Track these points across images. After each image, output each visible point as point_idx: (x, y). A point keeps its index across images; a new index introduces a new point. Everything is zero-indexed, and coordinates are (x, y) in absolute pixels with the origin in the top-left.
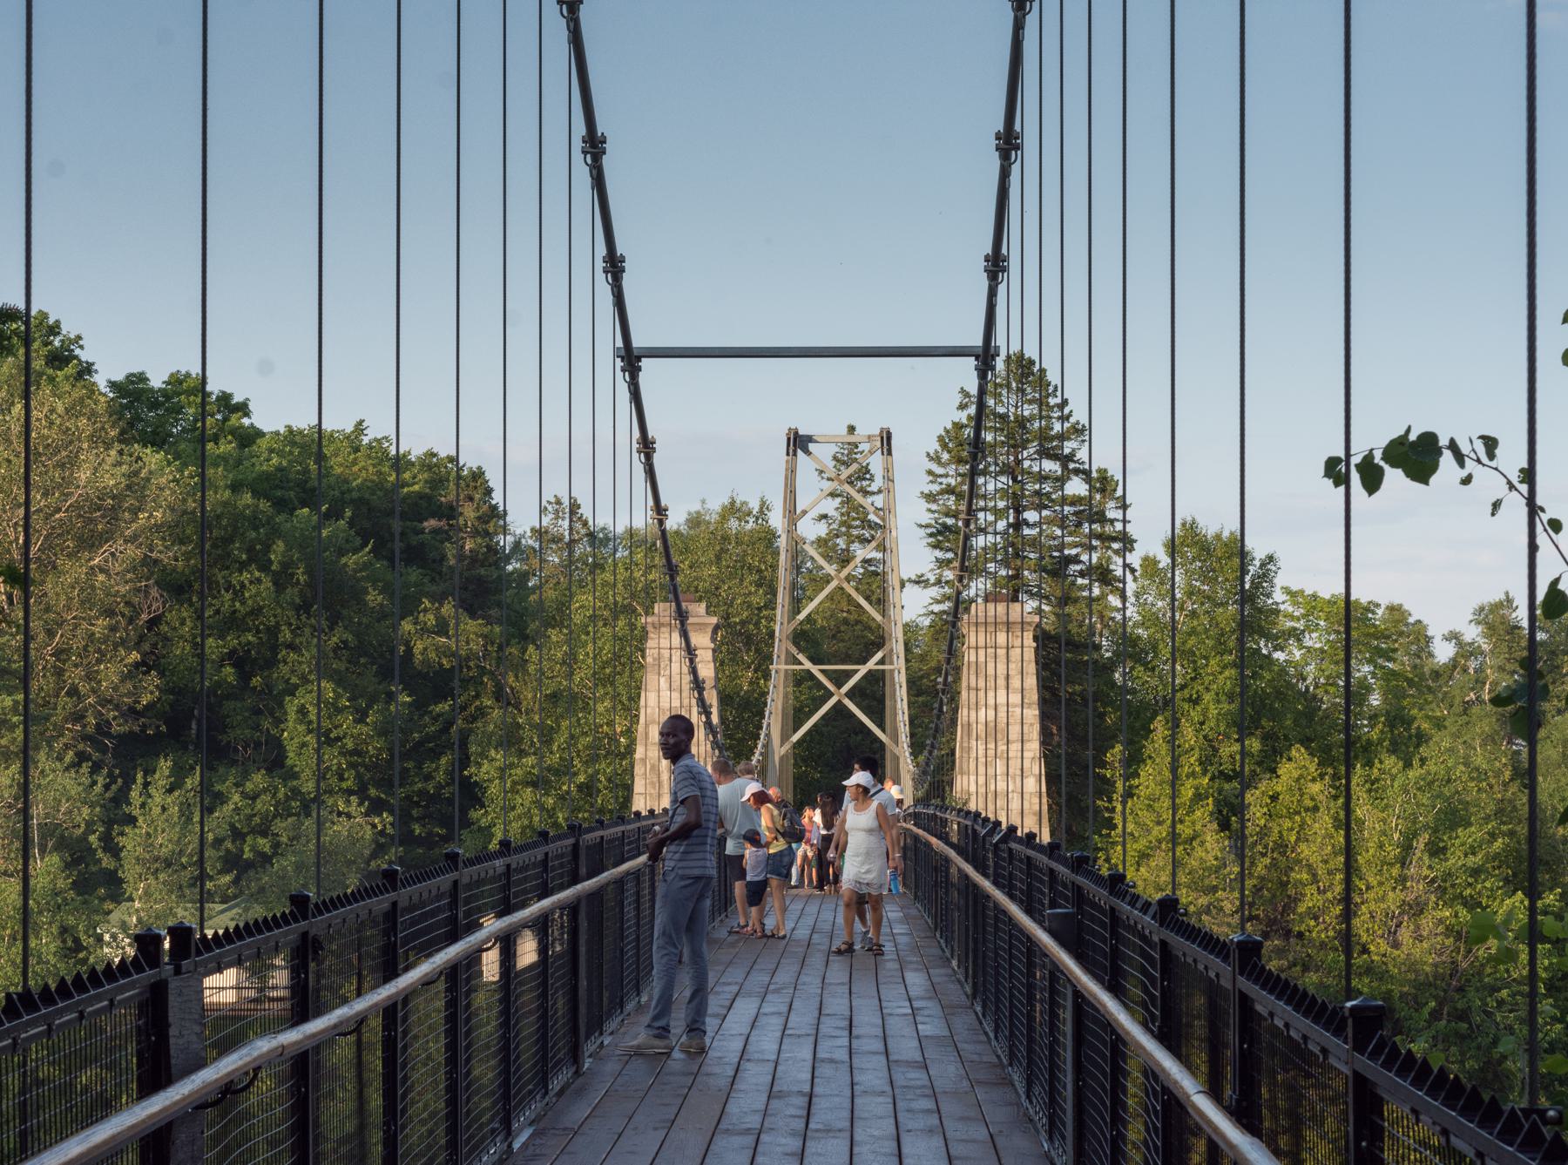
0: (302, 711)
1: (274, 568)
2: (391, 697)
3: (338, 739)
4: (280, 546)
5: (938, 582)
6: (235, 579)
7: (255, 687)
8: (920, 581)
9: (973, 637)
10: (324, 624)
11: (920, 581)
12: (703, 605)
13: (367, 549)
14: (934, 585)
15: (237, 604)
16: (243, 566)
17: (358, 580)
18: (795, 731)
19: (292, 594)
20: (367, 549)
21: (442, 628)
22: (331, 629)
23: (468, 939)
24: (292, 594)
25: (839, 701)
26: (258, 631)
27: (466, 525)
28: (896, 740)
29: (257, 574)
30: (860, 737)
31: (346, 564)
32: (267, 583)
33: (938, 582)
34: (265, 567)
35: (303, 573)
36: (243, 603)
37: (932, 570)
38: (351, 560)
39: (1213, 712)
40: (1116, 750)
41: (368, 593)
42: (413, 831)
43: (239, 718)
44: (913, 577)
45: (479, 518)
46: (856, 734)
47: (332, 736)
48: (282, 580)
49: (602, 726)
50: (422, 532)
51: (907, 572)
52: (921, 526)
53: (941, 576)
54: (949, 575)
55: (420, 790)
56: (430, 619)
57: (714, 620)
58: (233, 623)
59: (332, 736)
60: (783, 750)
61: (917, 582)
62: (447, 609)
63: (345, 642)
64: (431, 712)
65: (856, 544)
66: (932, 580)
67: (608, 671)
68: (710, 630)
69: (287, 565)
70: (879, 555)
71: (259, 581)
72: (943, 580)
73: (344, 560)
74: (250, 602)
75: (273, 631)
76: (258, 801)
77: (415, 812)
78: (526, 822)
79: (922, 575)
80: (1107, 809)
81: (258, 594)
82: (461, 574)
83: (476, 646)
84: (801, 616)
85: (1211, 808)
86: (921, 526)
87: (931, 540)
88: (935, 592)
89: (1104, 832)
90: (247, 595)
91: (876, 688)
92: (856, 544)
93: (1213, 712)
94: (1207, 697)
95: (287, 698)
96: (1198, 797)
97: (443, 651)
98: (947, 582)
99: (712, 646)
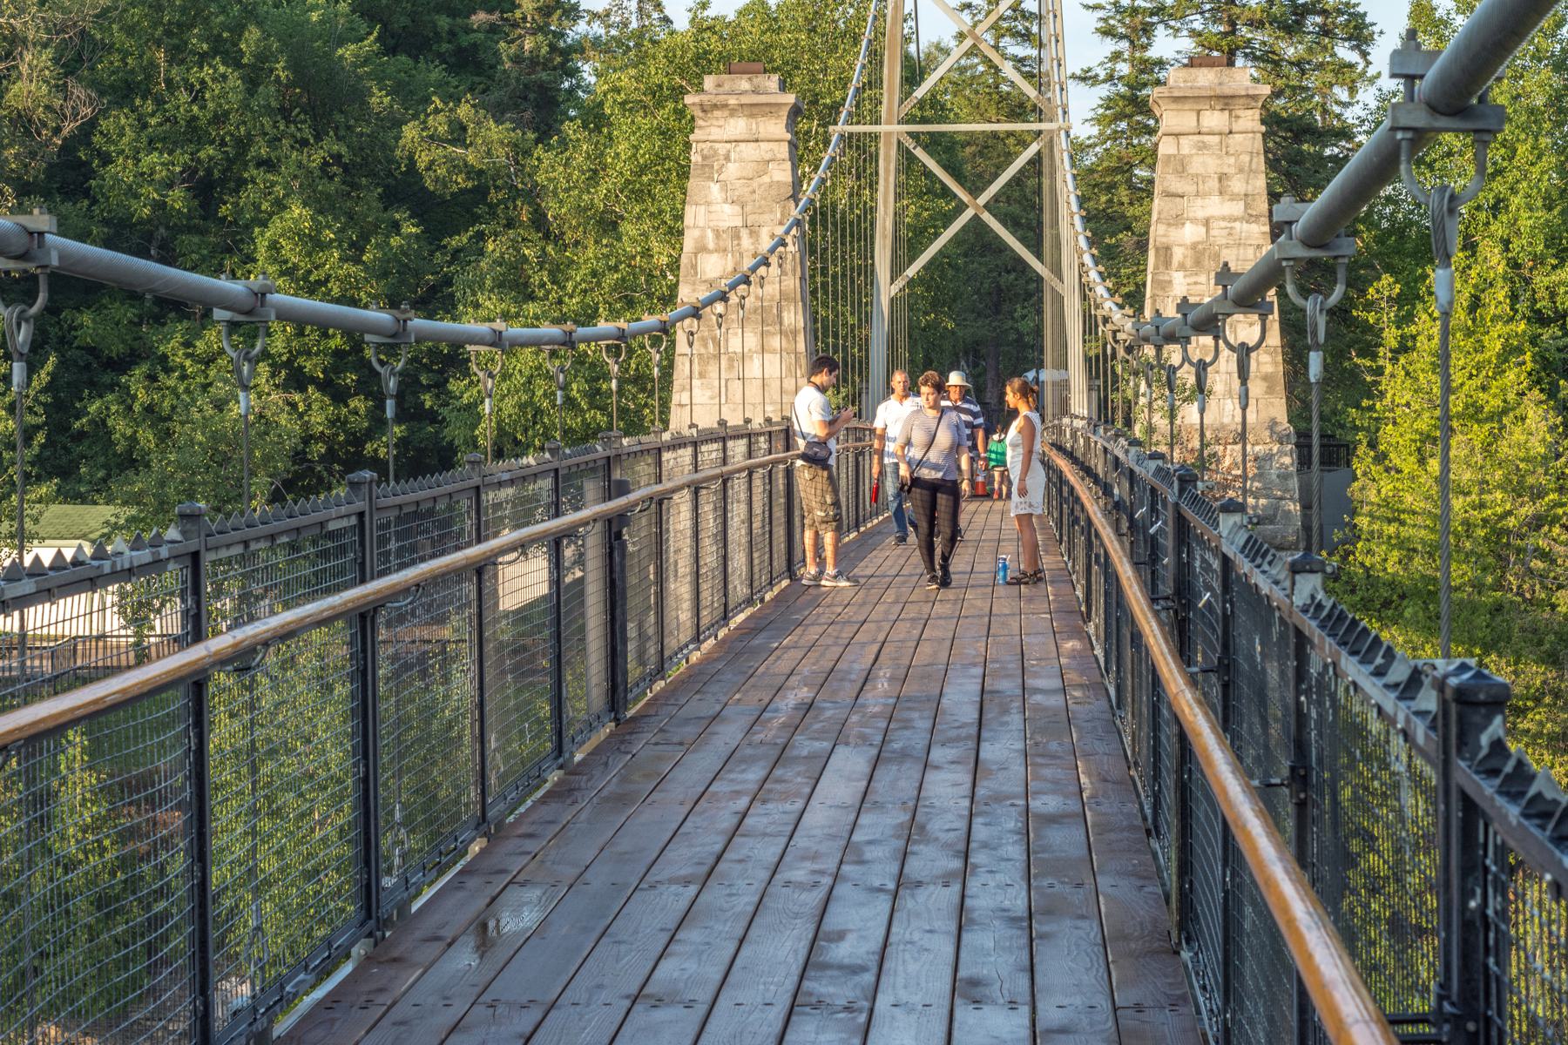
0: (274, 246)
1: (245, 61)
2: (396, 227)
3: (320, 283)
4: (253, 34)
5: (1110, 78)
6: (194, 75)
7: (225, 217)
8: (1086, 78)
9: (1171, 119)
10: (307, 133)
11: (1086, 78)
12: (775, 78)
13: (372, 38)
14: (1104, 81)
15: (195, 108)
16: (203, 59)
17: (360, 78)
18: (911, 262)
19: (268, 94)
20: (372, 38)
21: (458, 134)
22: (318, 138)
23: (264, 628)
24: (268, 94)
25: (976, 218)
26: (223, 143)
27: (524, 19)
28: (1057, 271)
29: (222, 69)
30: (1012, 276)
31: (341, 57)
32: (235, 80)
33: (1110, 78)
34: (234, 61)
35: (284, 69)
36: (203, 107)
37: (1102, 64)
38: (347, 52)
39: (1525, 223)
40: (1384, 282)
41: (373, 95)
42: (423, 403)
43: (194, 256)
44: (1078, 72)
45: (539, 9)
46: (1008, 272)
47: (312, 278)
48: (254, 78)
49: (634, 257)
50: (468, 30)
51: (1074, 66)
52: (1087, 7)
53: (1113, 70)
54: (1124, 68)
55: (430, 350)
56: (440, 125)
57: (790, 98)
58: (194, 133)
59: (312, 278)
60: (894, 289)
61: (1084, 79)
62: (464, 111)
63: (338, 158)
64: (445, 247)
65: (1007, 39)
66: (1102, 75)
67: (645, 179)
68: (784, 113)
69: (263, 57)
70: (1034, 53)
71: (224, 77)
72: (1116, 75)
73: (340, 51)
74: (211, 105)
75: (243, 144)
76: (212, 366)
77: (424, 380)
78: (524, 398)
79: (1090, 70)
80: (1371, 370)
81: (224, 95)
82: (518, 80)
83: (501, 155)
84: (920, 92)
85: (1529, 366)
86: (1087, 7)
87: (1101, 24)
88: (1104, 90)
89: (1365, 403)
90: (207, 96)
91: (1032, 216)
92: (1007, 39)
93: (1525, 223)
94: (1516, 201)
95: (257, 230)
96: (1510, 351)
97: (456, 166)
98: (1120, 78)
99: (789, 136)
